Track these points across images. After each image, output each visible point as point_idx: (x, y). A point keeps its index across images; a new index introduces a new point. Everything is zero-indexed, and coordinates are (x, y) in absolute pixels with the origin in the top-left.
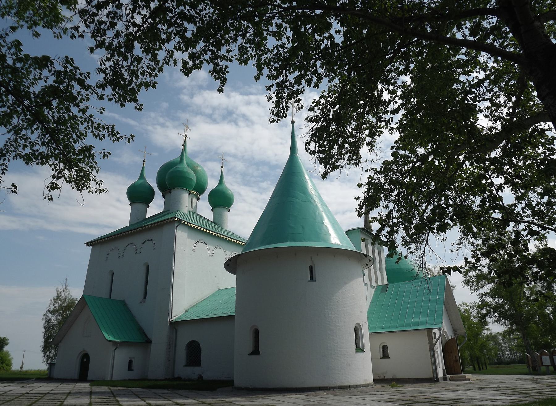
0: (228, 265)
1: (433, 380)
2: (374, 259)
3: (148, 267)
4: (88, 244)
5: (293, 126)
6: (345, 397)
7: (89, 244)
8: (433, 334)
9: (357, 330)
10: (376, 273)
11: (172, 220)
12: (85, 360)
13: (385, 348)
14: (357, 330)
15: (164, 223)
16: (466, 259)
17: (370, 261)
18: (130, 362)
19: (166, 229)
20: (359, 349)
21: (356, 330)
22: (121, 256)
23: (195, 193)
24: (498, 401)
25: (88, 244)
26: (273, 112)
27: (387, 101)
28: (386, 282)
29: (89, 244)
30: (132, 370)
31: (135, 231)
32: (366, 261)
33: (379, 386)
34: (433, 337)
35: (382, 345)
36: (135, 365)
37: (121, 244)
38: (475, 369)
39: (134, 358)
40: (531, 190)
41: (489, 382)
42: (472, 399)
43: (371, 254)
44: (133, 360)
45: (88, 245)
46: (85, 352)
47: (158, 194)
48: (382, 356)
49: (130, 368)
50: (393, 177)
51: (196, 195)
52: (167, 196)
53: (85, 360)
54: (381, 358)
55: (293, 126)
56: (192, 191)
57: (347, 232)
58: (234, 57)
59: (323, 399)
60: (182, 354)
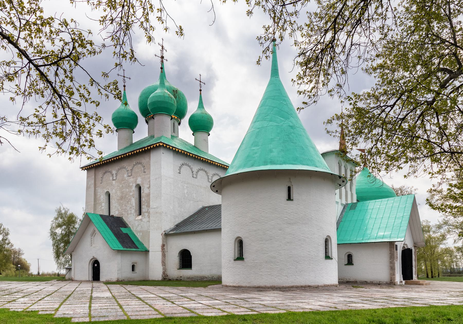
1: (391, 284)
5: (201, 94)
6: (315, 294)
7: (84, 168)
8: (395, 246)
9: (327, 241)
10: (346, 192)
12: (96, 265)
14: (327, 241)
15: (151, 147)
16: (413, 187)
20: (328, 257)
23: (176, 118)
24: (448, 300)
28: (355, 201)
29: (84, 168)
31: (125, 155)
32: (340, 182)
33: (343, 286)
34: (395, 249)
35: (348, 254)
36: (137, 269)
38: (428, 277)
41: (445, 285)
42: (424, 298)
44: (135, 264)
45: (83, 169)
47: (141, 119)
50: (453, 53)
51: (177, 121)
52: (151, 122)
53: (96, 265)
55: (201, 94)
56: (174, 116)
58: (155, 10)
59: (297, 294)
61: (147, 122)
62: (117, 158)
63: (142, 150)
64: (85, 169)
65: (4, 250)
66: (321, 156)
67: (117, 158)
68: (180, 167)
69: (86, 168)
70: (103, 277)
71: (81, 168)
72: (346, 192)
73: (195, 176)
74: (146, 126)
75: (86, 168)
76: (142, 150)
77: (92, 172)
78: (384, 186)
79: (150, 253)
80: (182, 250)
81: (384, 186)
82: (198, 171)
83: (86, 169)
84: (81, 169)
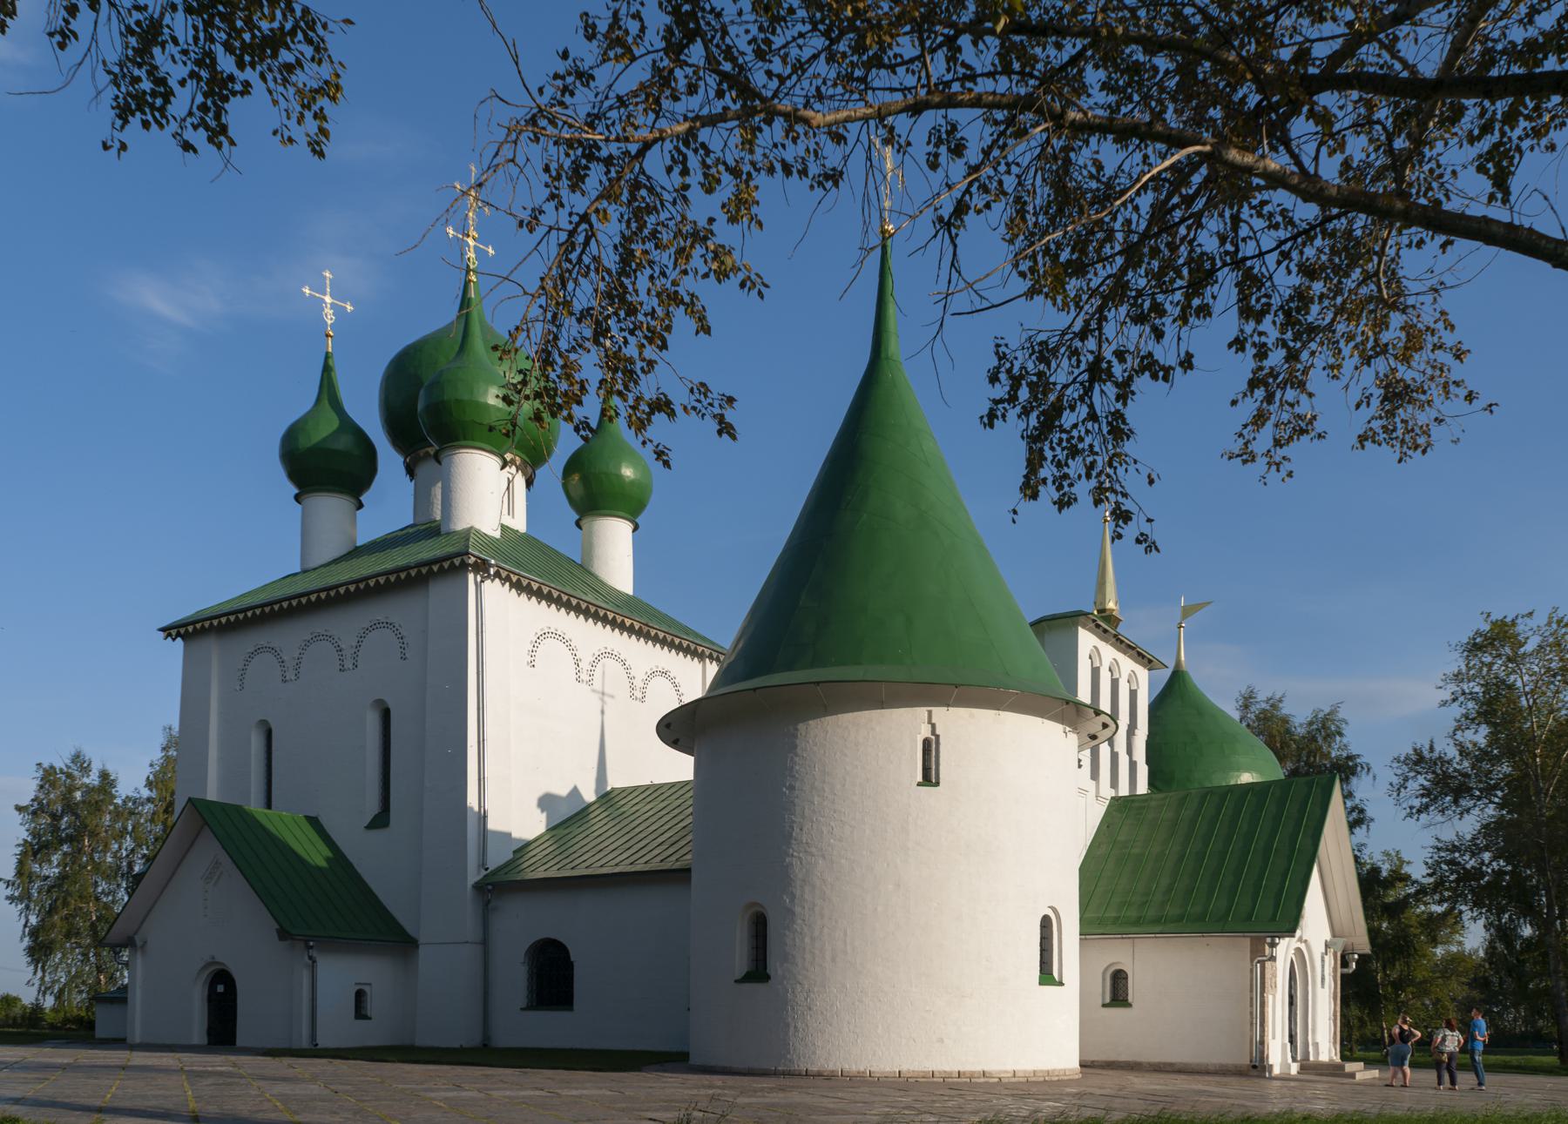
0: (668, 726)
2: (1114, 716)
3: (386, 715)
4: (171, 631)
7: (174, 632)
10: (1114, 757)
11: (457, 561)
13: (1118, 980)
17: (1105, 726)
18: (360, 995)
19: (438, 591)
20: (1047, 975)
21: (1046, 923)
22: (290, 675)
25: (171, 631)
26: (1427, 864)
27: (1418, 871)
29: (174, 632)
30: (366, 1017)
36: (373, 1005)
37: (288, 637)
39: (370, 984)
40: (1480, 749)
43: (1105, 705)
44: (367, 989)
45: (169, 635)
46: (761, 909)
47: (389, 460)
48: (1108, 1000)
49: (360, 1012)
53: (220, 988)
54: (1104, 1005)
57: (1032, 625)
60: (514, 978)
61: (411, 471)
62: (241, 616)
63: (398, 577)
64: (178, 635)
65: (1362, 266)
66: (1030, 629)
67: (304, 600)
68: (535, 645)
69: (182, 631)
70: (245, 1032)
71: (162, 630)
72: (1114, 757)
73: (584, 677)
74: (409, 486)
75: (182, 631)
76: (398, 577)
77: (212, 648)
78: (1246, 943)
79: (422, 950)
80: (538, 941)
81: (1246, 943)
82: (597, 659)
83: (182, 638)
84: (162, 634)
